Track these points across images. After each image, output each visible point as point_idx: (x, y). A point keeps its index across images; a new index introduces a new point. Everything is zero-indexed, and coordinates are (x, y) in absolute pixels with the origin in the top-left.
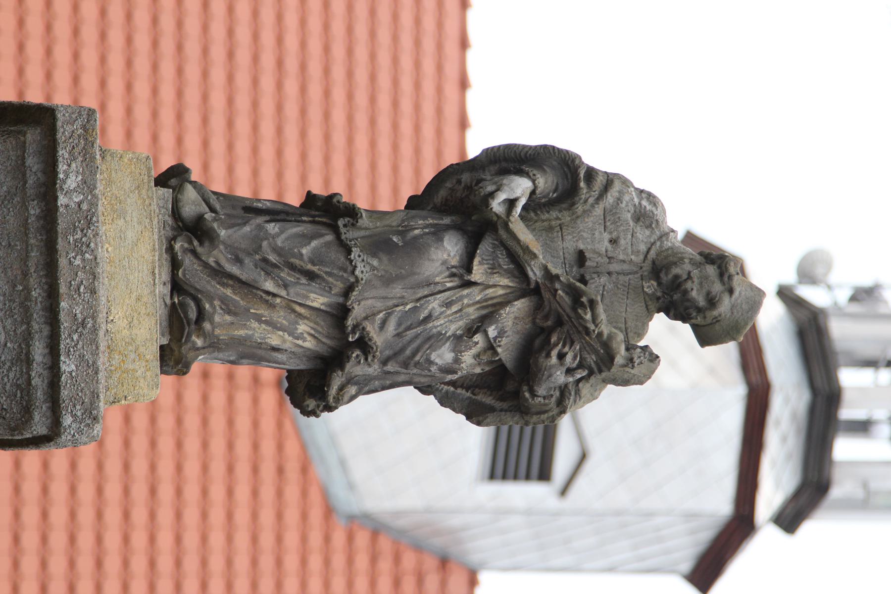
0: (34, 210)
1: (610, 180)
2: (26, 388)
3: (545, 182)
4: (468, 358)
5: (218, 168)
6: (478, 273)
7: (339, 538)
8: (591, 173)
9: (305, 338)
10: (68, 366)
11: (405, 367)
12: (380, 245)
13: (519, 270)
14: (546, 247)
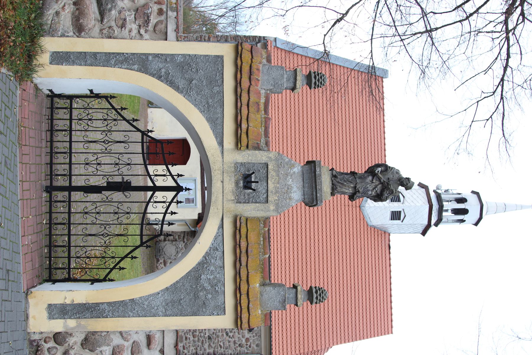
0: (313, 174)
1: (392, 168)
2: (313, 198)
3: (383, 168)
4: (373, 193)
5: (338, 168)
6: (374, 181)
7: (369, 229)
8: (390, 167)
9: (351, 191)
10: (318, 195)
11: (365, 194)
12: (360, 178)
13: (380, 181)
14: (384, 177)
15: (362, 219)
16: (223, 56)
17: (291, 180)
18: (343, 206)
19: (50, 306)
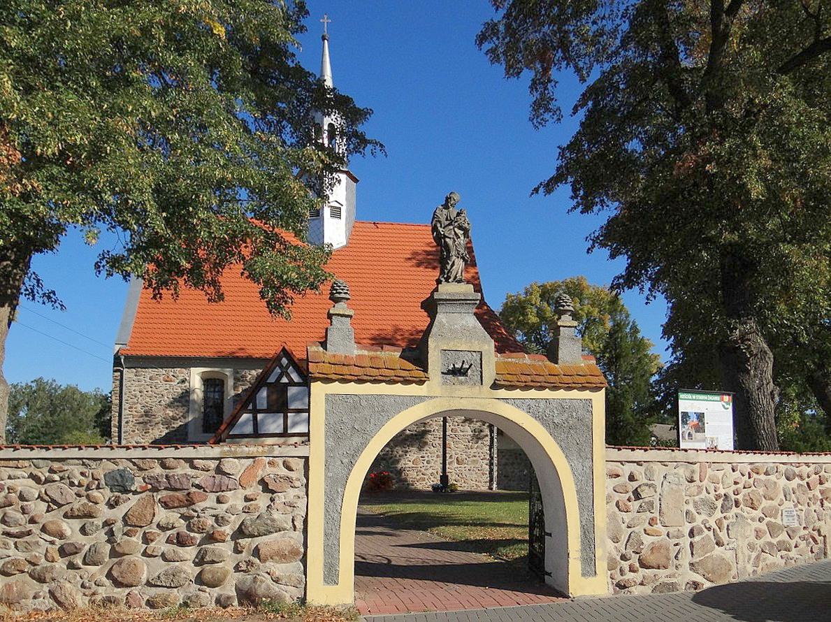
17: (456, 326)
19: (583, 575)
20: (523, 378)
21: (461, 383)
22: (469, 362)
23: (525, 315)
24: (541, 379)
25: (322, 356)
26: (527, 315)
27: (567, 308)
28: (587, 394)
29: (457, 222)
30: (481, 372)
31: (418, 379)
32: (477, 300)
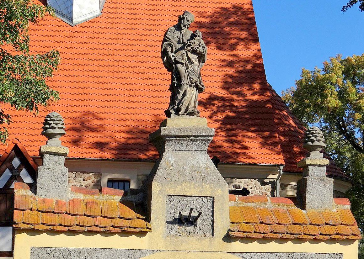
15: (91, 24)
16: (32, 248)
17: (185, 167)
18: (72, 51)
20: (262, 228)
21: (189, 234)
22: (199, 209)
23: (323, 96)
24: (283, 229)
25: (30, 201)
26: (327, 97)
27: (316, 143)
28: (336, 248)
29: (189, 45)
30: (213, 221)
31: (137, 230)
32: (210, 136)
